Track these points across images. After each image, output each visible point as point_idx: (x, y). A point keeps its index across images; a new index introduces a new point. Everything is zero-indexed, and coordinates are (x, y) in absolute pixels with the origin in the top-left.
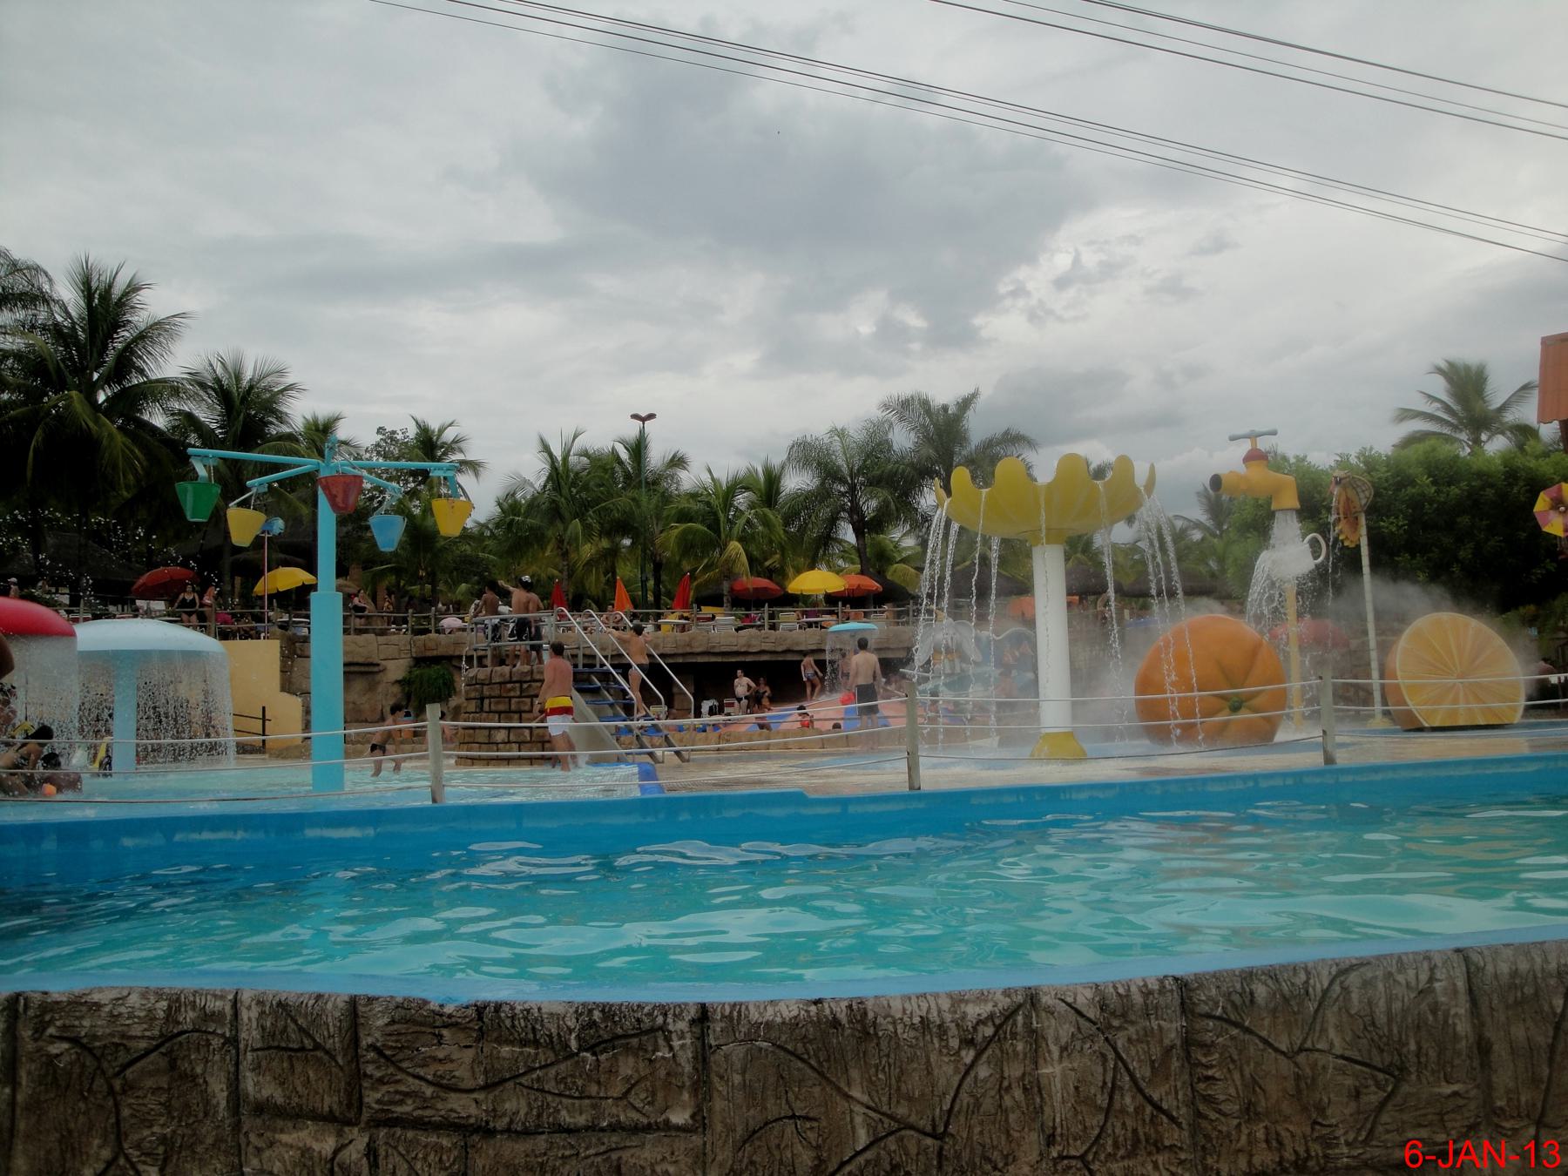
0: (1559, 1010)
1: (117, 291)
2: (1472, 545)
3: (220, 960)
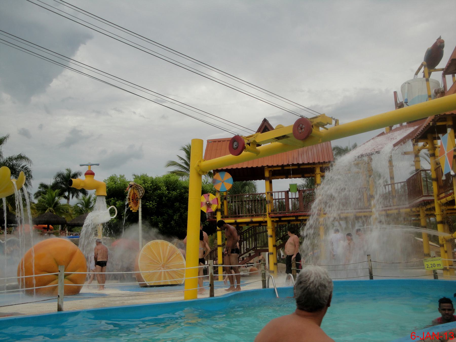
0: (95, 190)
1: (134, 177)
2: (179, 214)
3: (14, 187)
